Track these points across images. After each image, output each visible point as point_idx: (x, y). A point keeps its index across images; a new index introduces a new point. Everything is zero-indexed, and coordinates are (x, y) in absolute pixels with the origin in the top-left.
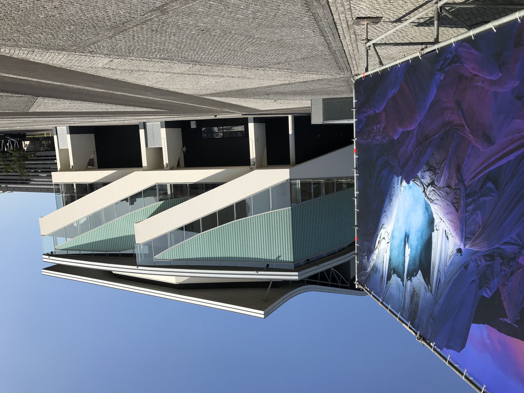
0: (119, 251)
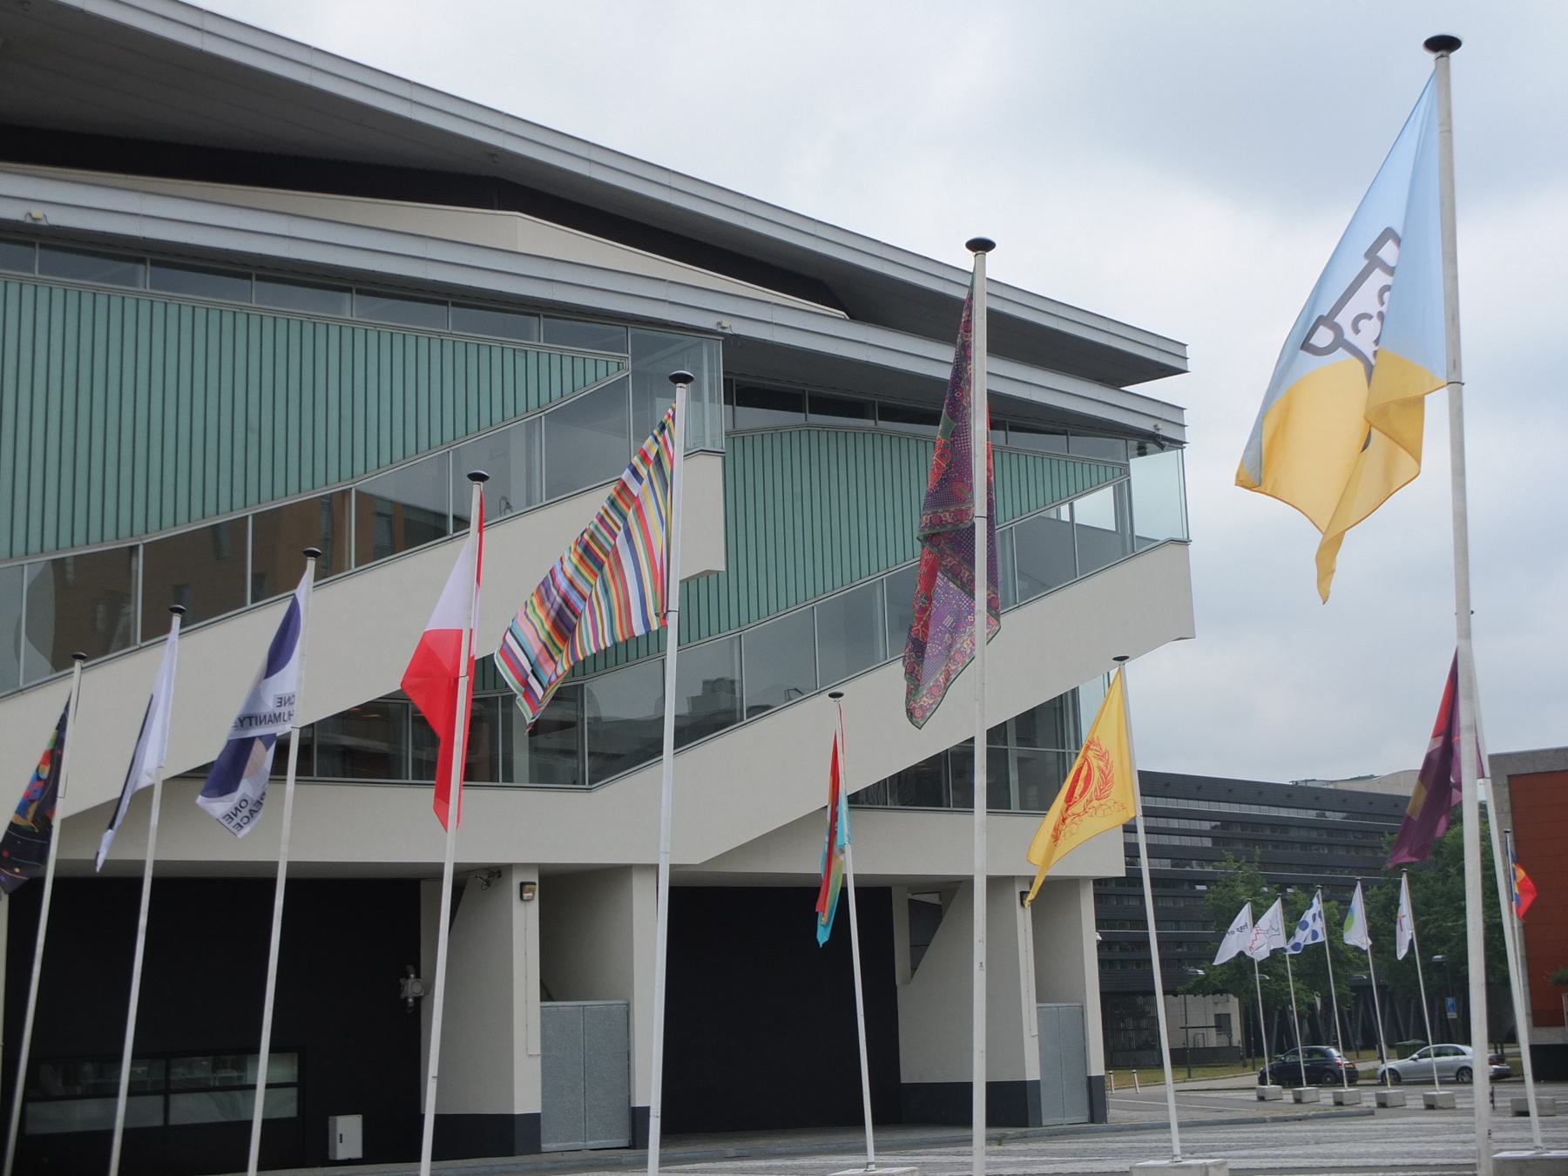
0: (809, 428)
